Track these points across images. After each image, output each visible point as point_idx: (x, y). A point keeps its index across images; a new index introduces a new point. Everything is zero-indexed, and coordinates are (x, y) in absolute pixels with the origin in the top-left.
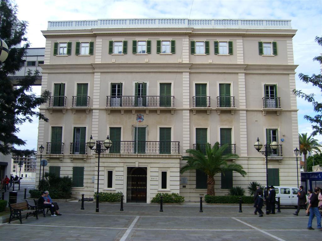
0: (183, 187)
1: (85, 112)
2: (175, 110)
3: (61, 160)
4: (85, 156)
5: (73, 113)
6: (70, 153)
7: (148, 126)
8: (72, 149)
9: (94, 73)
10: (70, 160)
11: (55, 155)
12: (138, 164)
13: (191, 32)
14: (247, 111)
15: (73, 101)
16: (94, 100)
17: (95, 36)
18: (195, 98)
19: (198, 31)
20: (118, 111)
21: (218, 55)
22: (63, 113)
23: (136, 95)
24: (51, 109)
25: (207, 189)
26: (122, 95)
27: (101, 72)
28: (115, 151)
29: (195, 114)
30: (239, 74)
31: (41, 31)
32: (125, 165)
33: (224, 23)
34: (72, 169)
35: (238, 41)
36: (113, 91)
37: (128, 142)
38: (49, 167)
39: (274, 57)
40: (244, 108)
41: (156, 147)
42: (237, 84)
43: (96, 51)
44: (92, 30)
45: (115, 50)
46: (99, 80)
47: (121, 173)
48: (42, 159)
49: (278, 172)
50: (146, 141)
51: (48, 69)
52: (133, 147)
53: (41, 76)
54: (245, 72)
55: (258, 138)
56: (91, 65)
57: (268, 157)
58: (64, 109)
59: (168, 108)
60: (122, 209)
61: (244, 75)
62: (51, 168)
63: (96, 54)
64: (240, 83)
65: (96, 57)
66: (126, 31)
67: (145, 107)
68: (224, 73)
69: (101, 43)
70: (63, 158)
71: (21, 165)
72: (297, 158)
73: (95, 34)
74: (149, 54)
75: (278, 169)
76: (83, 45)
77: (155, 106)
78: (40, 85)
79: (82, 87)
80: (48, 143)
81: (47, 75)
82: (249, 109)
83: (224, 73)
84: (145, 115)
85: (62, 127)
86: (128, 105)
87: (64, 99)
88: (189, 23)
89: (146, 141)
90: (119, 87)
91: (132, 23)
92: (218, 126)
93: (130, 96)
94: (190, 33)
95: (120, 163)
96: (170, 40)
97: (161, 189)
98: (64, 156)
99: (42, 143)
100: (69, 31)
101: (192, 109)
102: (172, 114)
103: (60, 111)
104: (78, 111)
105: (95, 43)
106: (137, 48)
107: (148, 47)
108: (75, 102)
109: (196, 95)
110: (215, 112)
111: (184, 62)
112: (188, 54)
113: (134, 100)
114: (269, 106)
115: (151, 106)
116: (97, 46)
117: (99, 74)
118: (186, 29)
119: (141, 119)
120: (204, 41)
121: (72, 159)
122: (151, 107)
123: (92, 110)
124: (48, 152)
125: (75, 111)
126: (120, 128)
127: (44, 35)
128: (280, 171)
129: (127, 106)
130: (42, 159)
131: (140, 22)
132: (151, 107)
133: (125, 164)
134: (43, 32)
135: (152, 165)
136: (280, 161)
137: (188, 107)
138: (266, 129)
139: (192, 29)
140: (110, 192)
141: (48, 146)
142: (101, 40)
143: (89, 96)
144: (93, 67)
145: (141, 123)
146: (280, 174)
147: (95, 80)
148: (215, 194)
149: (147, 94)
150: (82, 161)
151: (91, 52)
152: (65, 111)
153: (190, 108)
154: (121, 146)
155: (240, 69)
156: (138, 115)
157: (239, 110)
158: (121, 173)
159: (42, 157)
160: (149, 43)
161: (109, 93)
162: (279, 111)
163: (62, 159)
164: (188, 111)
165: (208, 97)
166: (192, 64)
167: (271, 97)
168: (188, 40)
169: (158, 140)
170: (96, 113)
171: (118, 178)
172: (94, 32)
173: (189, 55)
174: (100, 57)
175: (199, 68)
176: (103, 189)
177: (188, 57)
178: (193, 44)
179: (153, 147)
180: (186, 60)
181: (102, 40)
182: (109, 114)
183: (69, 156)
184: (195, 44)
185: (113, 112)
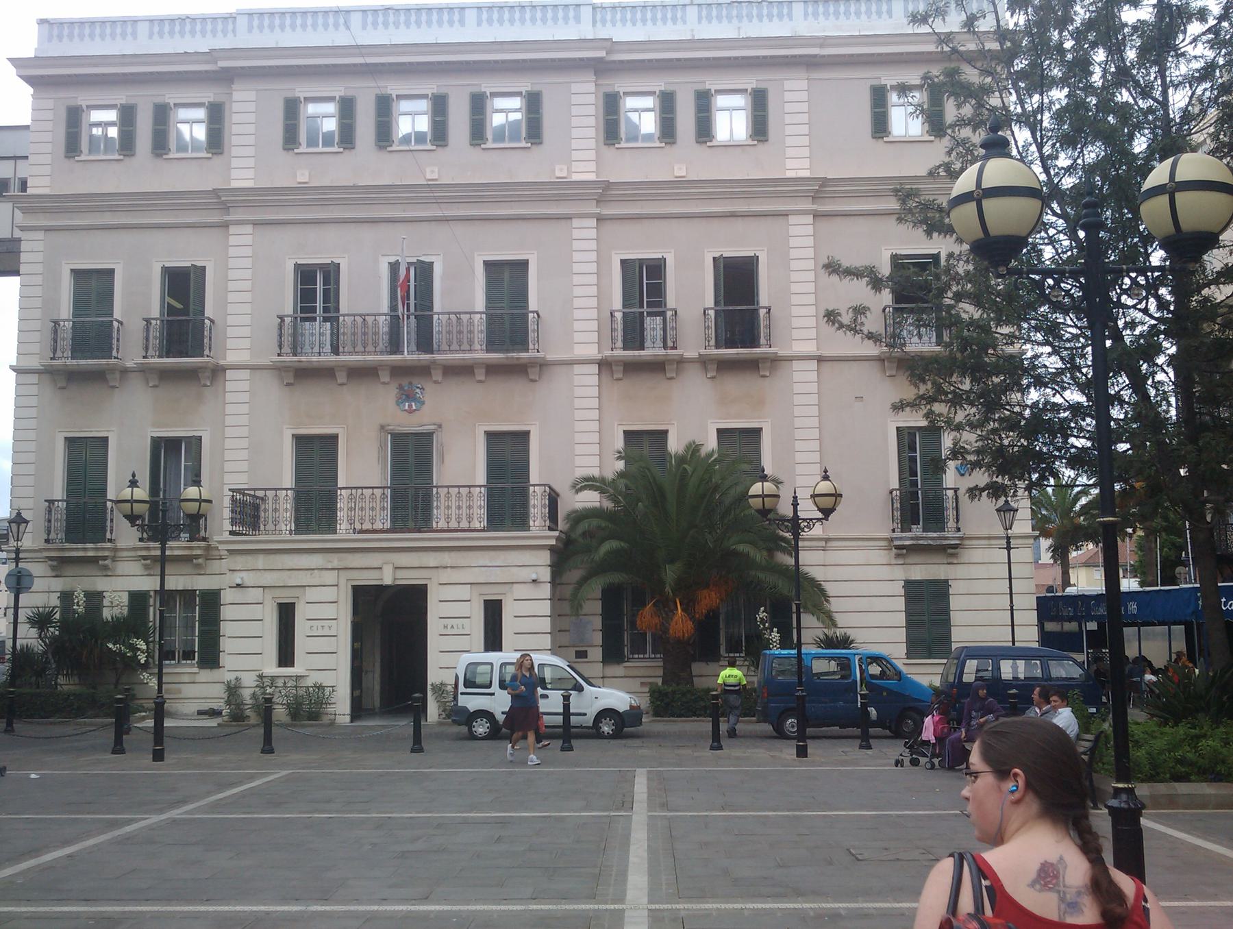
1: (198, 379)
2: (541, 366)
3: (106, 568)
4: (199, 548)
5: (59, 385)
6: (141, 540)
7: (440, 426)
9: (225, 226)
11: (80, 546)
12: (394, 573)
13: (602, 54)
14: (820, 359)
15: (147, 339)
16: (230, 332)
17: (227, 77)
18: (712, 313)
19: (631, 51)
20: (322, 374)
21: (709, 144)
22: (111, 384)
24: (59, 371)
25: (945, 661)
26: (337, 310)
27: (255, 224)
28: (411, 524)
29: (620, 376)
30: (793, 219)
31: (13, 61)
32: (342, 582)
33: (735, 12)
35: (788, 85)
36: (305, 297)
37: (354, 491)
38: (59, 594)
39: (432, 154)
40: (810, 348)
41: (459, 508)
43: (235, 140)
44: (212, 55)
45: (770, 123)
46: (248, 251)
47: (330, 611)
49: (947, 595)
50: (434, 484)
51: (44, 211)
53: (19, 240)
54: (815, 207)
55: (134, 475)
56: (215, 193)
57: (170, 544)
58: (112, 370)
59: (512, 358)
60: (417, 747)
61: (810, 219)
63: (235, 151)
64: (794, 253)
65: (235, 163)
66: (404, 54)
67: (427, 357)
68: (733, 215)
69: (804, 96)
70: (114, 559)
72: (1008, 538)
73: (225, 70)
74: (440, 149)
75: (946, 581)
76: (405, 105)
77: (464, 351)
78: (16, 273)
79: (94, 283)
80: (51, 502)
81: (40, 235)
82: (826, 352)
83: (733, 215)
84: (429, 387)
85: (106, 440)
86: (360, 348)
88: (598, 17)
89: (434, 484)
90: (326, 281)
91: (375, 24)
92: (709, 421)
93: (368, 315)
94: (600, 60)
95: (324, 572)
96: (337, 95)
97: (272, 669)
98: (115, 550)
100: (123, 59)
101: (609, 359)
102: (532, 381)
103: (98, 376)
104: (167, 376)
105: (227, 106)
106: (713, 117)
108: (154, 342)
109: (624, 306)
110: (697, 365)
111: (576, 177)
116: (236, 118)
117: (249, 229)
118: (583, 43)
120: (749, 87)
121: (149, 562)
122: (449, 356)
123: (223, 369)
125: (291, 374)
126: (334, 438)
127: (20, 76)
129: (357, 353)
131: (435, 16)
132: (449, 356)
133: (344, 575)
135: (445, 576)
136: (950, 551)
137: (592, 352)
138: (898, 428)
139: (609, 44)
142: (252, 95)
143: (116, 320)
144: (224, 203)
146: (955, 602)
147: (232, 252)
148: (695, 679)
149: (437, 307)
150: (187, 569)
151: (760, 129)
152: (118, 375)
153: (599, 357)
154: (532, 502)
155: (793, 196)
156: (401, 387)
157: (790, 359)
158: (330, 611)
159: (21, 555)
160: (439, 106)
161: (288, 304)
162: (766, 359)
163: (106, 562)
164: (595, 368)
165: (765, 308)
166: (608, 186)
167: (303, 315)
168: (591, 87)
170: (237, 384)
171: (254, 629)
172: (222, 64)
173: (597, 150)
174: (806, 152)
175: (633, 199)
177: (592, 155)
178: (611, 104)
180: (584, 172)
181: (254, 92)
182: (288, 385)
183: (135, 549)
184: (621, 101)
185: (304, 375)
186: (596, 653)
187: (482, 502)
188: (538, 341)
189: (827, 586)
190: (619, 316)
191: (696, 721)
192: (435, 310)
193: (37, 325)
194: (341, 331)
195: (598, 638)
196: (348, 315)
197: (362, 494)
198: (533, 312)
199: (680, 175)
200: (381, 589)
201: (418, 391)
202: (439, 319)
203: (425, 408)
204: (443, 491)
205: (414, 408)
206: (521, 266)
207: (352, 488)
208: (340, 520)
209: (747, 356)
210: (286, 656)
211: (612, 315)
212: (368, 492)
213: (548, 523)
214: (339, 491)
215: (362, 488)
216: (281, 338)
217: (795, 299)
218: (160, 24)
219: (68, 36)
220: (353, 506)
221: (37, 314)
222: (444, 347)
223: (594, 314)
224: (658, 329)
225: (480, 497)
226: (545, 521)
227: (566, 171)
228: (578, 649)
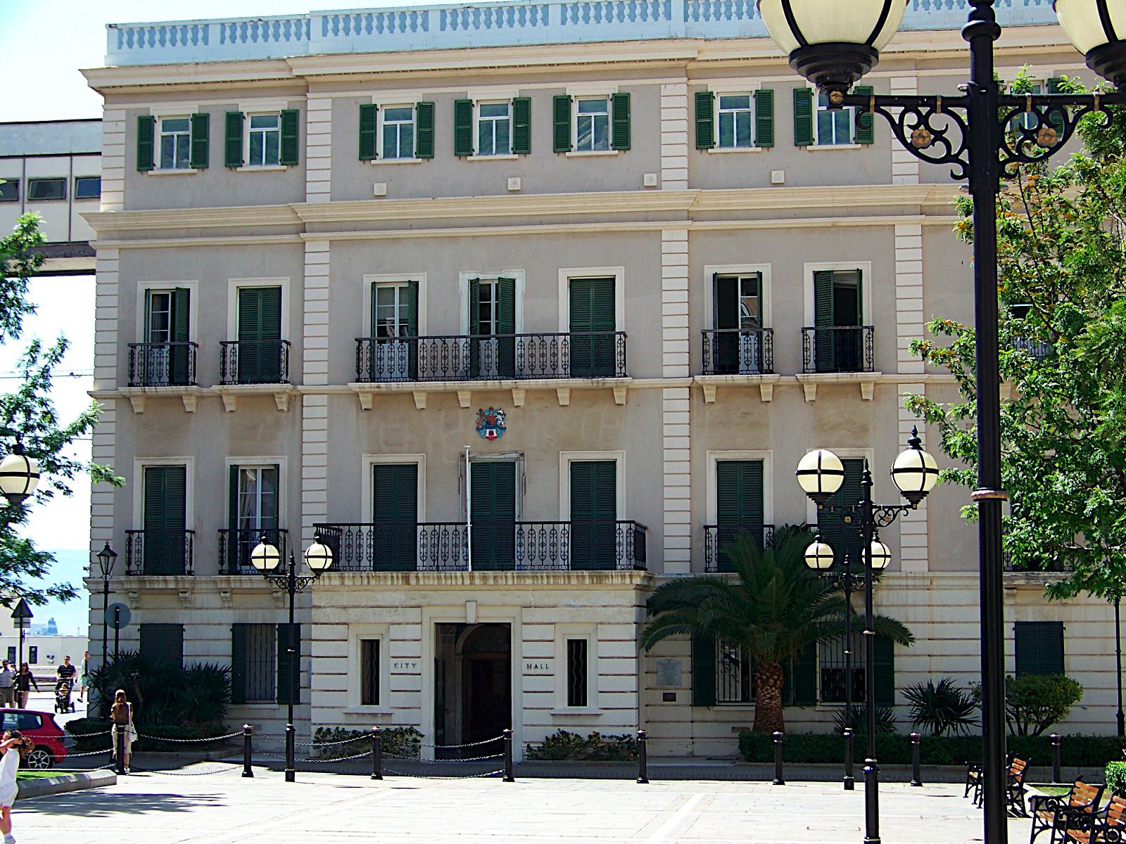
0: (664, 700)
6: (221, 573)
7: (522, 455)
8: (226, 554)
10: (268, 596)
23: (472, 329)
34: (230, 635)
37: (437, 527)
38: (139, 627)
39: (418, 167)
42: (889, 276)
43: (310, 152)
48: (112, 599)
52: (629, 544)
62: (147, 630)
71: (25, 619)
79: (592, 292)
87: (280, 352)
93: (448, 337)
99: (109, 534)
107: (204, 140)
112: (684, 150)
113: (464, 352)
114: (386, 374)
115: (392, 380)
119: (496, 426)
124: (133, 567)
128: (1065, 634)
130: (112, 599)
134: (91, 74)
140: (590, 731)
141: (134, 543)
143: (285, 342)
145: (496, 445)
167: (381, 338)
169: (565, 515)
176: (552, 712)
179: (532, 545)
186: (684, 696)
187: (566, 539)
188: (625, 365)
189: (911, 628)
190: (710, 336)
191: (744, 765)
192: (518, 331)
193: (113, 348)
194: (420, 354)
195: (686, 680)
196: (427, 338)
197: (445, 530)
198: (620, 333)
199: (650, 185)
200: (462, 626)
201: (499, 417)
202: (423, 344)
203: (507, 435)
204: (526, 528)
205: (495, 435)
206: (182, 296)
207: (434, 524)
208: (619, 554)
209: (253, 391)
210: (371, 694)
211: (704, 334)
212: (451, 528)
213: (633, 562)
214: (618, 525)
215: (445, 524)
216: (359, 362)
217: (901, 317)
218: (336, 22)
219: (571, 18)
220: (566, 542)
221: (114, 337)
222: (527, 371)
223: (685, 334)
224: (753, 351)
225: (564, 534)
226: (630, 560)
227: (779, 172)
228: (665, 692)
